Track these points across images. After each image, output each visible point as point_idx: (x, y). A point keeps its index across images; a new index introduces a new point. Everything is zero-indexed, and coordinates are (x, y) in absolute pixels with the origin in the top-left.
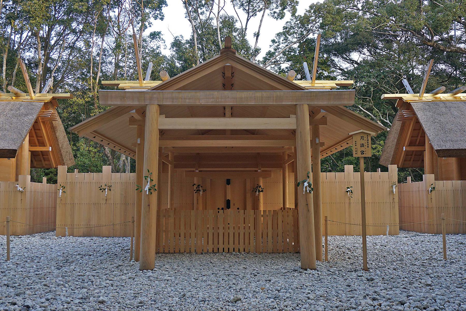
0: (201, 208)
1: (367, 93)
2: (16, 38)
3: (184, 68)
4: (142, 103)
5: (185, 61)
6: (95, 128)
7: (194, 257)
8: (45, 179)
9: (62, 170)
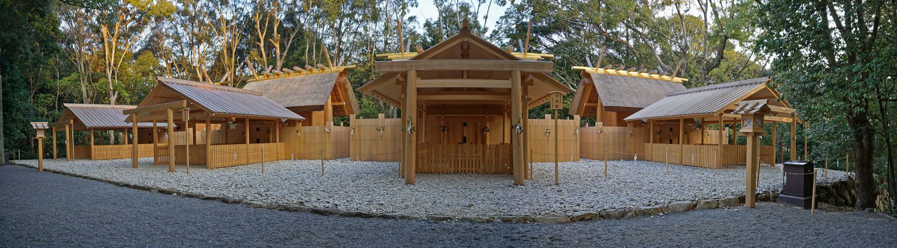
0: (446, 142)
1: (562, 65)
2: (320, 31)
3: (433, 43)
4: (405, 69)
5: (434, 37)
6: (373, 88)
7: (442, 176)
8: (342, 124)
9: (352, 117)
